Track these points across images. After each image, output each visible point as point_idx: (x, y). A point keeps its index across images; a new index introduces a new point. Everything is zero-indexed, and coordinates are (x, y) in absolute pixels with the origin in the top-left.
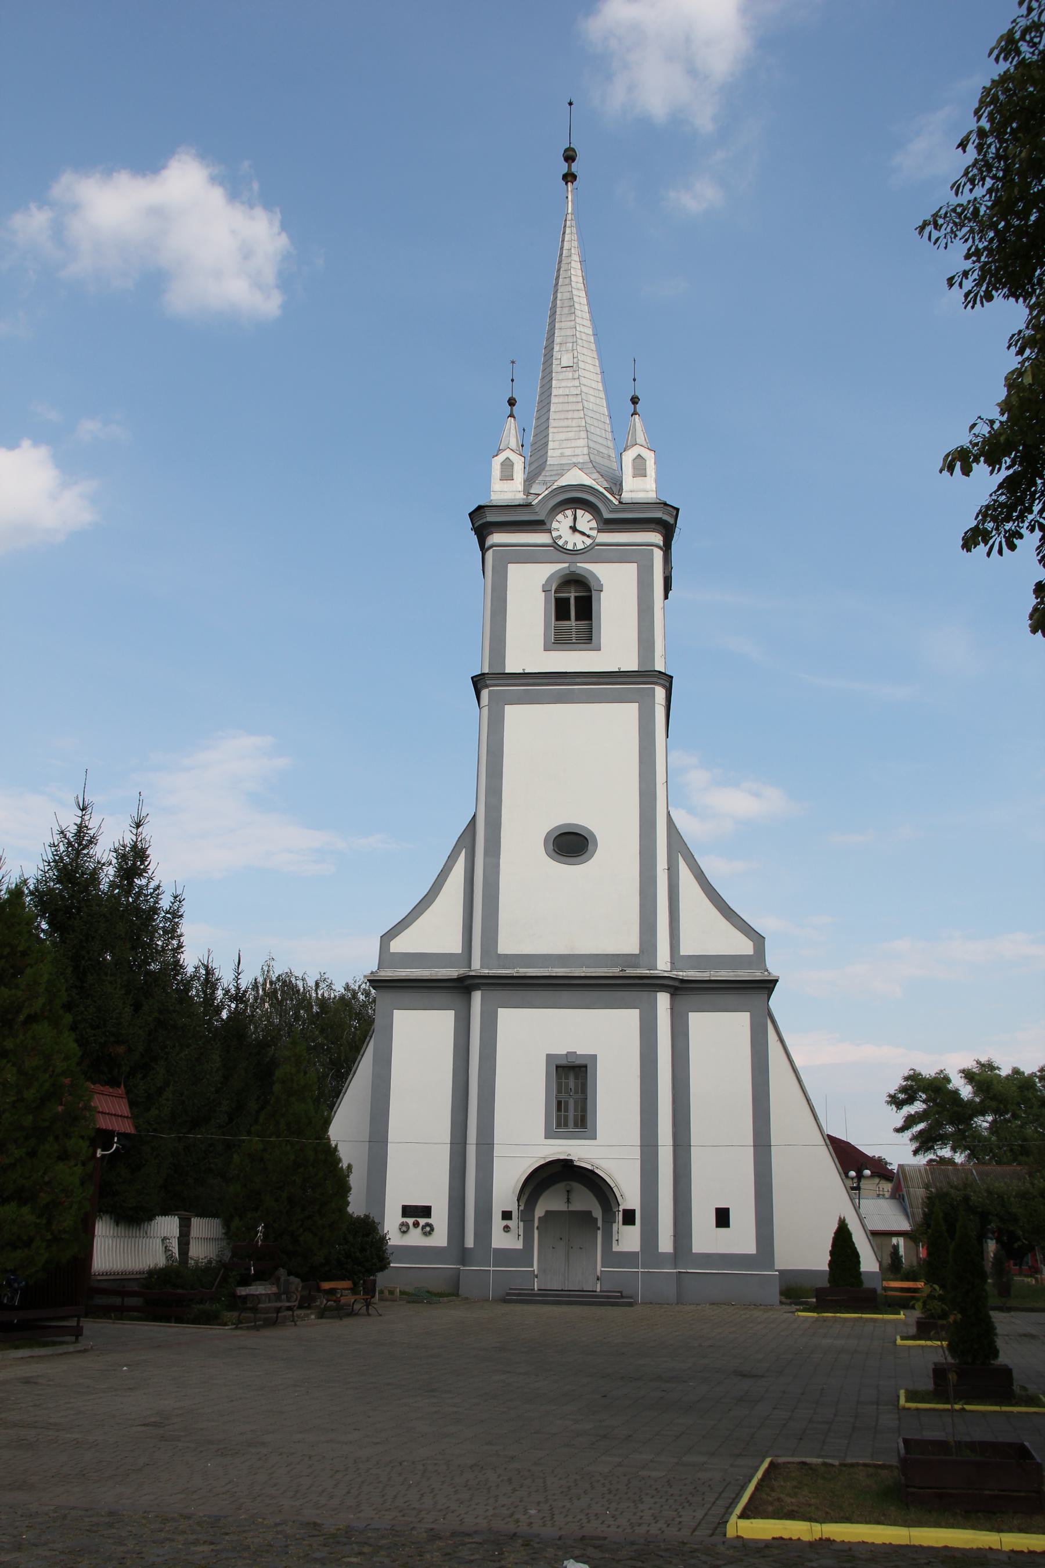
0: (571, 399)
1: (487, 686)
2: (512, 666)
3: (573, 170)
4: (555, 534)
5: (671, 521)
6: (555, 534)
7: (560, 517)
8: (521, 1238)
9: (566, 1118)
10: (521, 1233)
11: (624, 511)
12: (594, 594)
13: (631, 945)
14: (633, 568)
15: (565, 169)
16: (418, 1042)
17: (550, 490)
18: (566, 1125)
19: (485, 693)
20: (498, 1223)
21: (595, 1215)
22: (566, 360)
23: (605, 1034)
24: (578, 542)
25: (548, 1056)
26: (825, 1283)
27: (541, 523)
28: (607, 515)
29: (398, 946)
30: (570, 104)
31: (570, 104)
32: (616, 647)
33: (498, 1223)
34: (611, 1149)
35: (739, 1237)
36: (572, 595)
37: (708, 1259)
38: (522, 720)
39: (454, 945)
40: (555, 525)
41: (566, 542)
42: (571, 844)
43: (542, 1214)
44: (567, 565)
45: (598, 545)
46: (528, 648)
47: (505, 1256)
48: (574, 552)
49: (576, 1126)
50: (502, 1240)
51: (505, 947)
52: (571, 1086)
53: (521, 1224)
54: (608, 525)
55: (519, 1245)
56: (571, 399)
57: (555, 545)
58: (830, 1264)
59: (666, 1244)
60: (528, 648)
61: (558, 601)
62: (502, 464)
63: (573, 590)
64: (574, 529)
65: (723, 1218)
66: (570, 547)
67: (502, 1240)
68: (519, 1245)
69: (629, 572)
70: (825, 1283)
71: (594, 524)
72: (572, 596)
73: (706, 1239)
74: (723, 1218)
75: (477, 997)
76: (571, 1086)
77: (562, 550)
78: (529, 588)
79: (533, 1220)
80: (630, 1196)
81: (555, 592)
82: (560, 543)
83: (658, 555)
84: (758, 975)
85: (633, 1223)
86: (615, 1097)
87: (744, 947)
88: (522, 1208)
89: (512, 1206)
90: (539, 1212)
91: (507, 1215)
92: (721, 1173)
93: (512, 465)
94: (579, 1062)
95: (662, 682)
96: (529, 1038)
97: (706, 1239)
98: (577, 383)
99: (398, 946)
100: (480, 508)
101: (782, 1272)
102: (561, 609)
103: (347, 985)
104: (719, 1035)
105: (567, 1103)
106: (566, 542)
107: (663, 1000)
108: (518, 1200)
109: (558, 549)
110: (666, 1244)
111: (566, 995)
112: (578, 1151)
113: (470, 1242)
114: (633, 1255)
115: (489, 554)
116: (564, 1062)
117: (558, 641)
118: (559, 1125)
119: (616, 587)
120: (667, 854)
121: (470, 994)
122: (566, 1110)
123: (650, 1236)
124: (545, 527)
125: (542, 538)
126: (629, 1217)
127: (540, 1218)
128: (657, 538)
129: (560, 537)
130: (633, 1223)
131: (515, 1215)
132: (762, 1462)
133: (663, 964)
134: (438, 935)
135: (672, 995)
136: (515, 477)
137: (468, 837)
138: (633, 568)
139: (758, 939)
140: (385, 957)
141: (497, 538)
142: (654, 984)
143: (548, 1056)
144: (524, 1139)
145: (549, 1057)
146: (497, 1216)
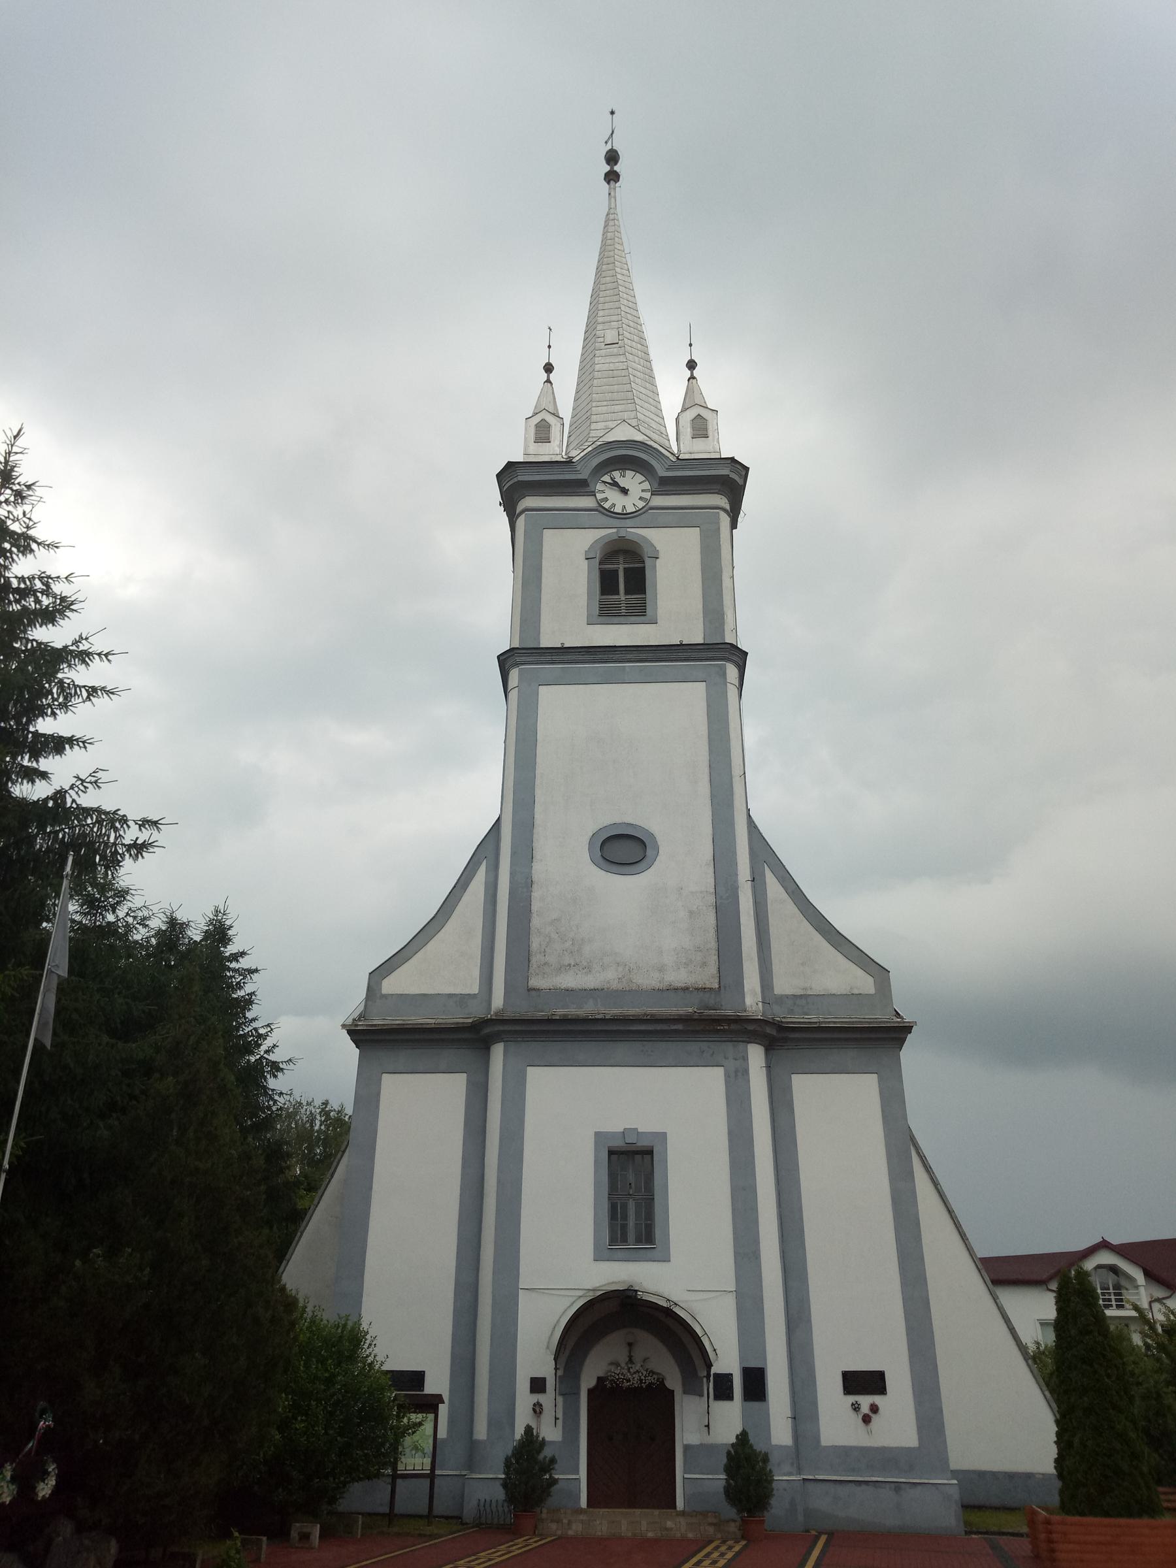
0: (619, 373)
1: (517, 665)
2: (547, 640)
3: (616, 168)
4: (599, 496)
5: (740, 482)
6: (599, 496)
8: (560, 1422)
9: (624, 1227)
10: (560, 1415)
11: (683, 468)
12: (648, 563)
13: (707, 976)
14: (778, 990)
15: (608, 168)
17: (594, 446)
18: (624, 1240)
19: (514, 675)
20: (524, 1400)
21: (669, 1384)
22: (611, 336)
23: (679, 1103)
24: (629, 503)
25: (597, 1134)
28: (662, 472)
29: (390, 986)
30: (612, 113)
31: (612, 113)
32: (675, 615)
33: (524, 1400)
34: (691, 1273)
35: (896, 1422)
37: (845, 1454)
38: (564, 706)
41: (614, 505)
42: (623, 849)
43: (592, 1383)
44: (614, 530)
45: (651, 508)
46: (570, 621)
48: (624, 516)
49: (638, 1240)
52: (631, 1181)
53: (560, 1399)
56: (619, 373)
60: (570, 621)
62: (537, 426)
63: (621, 560)
66: (618, 509)
71: (647, 486)
72: (621, 568)
75: (498, 1052)
76: (631, 1181)
77: (610, 513)
78: (571, 555)
79: (578, 1394)
80: (727, 1359)
81: (600, 563)
82: (607, 505)
83: (725, 520)
84: (880, 1016)
85: (729, 1397)
86: (694, 1196)
87: (865, 984)
88: (560, 1373)
89: (546, 1368)
91: (537, 1385)
92: (856, 1323)
93: (549, 426)
94: (644, 1143)
95: (735, 658)
96: (570, 1109)
97: (837, 1421)
98: (622, 358)
99: (390, 986)
100: (510, 465)
102: (607, 583)
103: (326, 1103)
104: (836, 1108)
105: (625, 1207)
106: (614, 505)
107: (756, 1055)
108: (556, 1359)
111: (621, 1049)
112: (652, 1278)
113: (481, 1432)
115: (521, 522)
116: (618, 1143)
117: (607, 612)
118: (613, 1241)
119: (673, 555)
120: (746, 868)
121: (488, 1049)
122: (625, 1217)
124: (588, 489)
127: (590, 1391)
128: (722, 501)
129: (606, 499)
130: (729, 1397)
131: (550, 1384)
133: (752, 1002)
134: (451, 975)
135: (768, 1050)
136: (552, 439)
138: (778, 990)
139: (880, 973)
141: (529, 502)
143: (597, 1134)
144: (563, 1261)
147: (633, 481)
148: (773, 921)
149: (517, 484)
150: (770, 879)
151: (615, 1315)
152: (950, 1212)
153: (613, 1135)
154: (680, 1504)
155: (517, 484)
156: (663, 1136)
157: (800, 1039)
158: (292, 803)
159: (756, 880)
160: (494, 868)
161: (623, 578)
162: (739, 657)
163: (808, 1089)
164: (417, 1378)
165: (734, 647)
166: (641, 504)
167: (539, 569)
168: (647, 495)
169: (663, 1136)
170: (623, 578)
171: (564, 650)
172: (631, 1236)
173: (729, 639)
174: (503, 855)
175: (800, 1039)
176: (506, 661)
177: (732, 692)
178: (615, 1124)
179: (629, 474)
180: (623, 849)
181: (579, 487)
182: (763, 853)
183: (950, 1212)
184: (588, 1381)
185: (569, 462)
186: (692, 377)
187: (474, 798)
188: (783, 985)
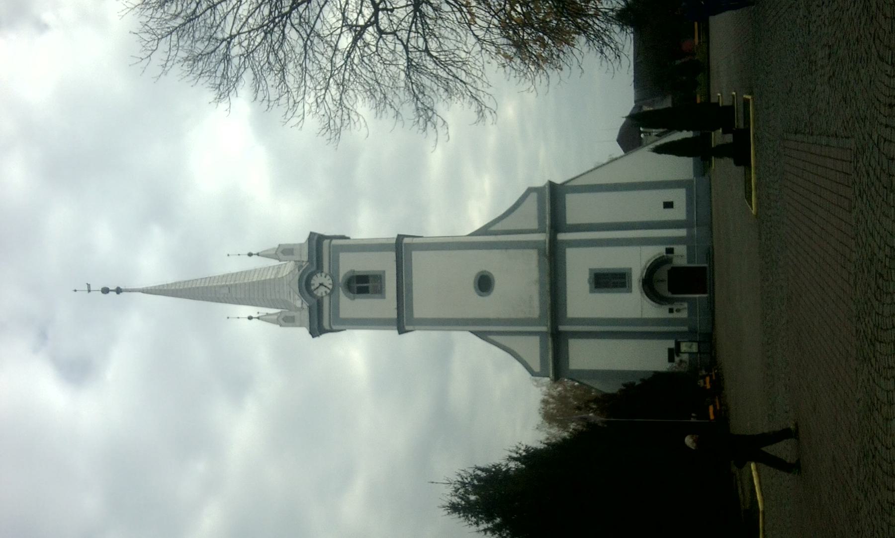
2: (394, 315)
5: (316, 237)
7: (331, 281)
13: (533, 254)
16: (585, 356)
20: (675, 315)
22: (226, 291)
23: (579, 264)
24: (328, 282)
26: (699, 159)
27: (318, 301)
28: (314, 268)
32: (385, 264)
33: (675, 315)
34: (635, 260)
35: (679, 196)
36: (355, 285)
37: (689, 212)
39: (535, 341)
40: (319, 295)
42: (484, 284)
47: (691, 311)
48: (334, 284)
49: (625, 278)
50: (684, 314)
51: (535, 313)
52: (607, 281)
54: (319, 268)
55: (686, 305)
57: (330, 295)
58: (689, 156)
59: (682, 232)
60: (387, 305)
61: (358, 293)
64: (321, 284)
65: (668, 205)
67: (684, 314)
68: (686, 305)
69: (344, 257)
70: (699, 159)
71: (319, 275)
73: (679, 213)
74: (668, 205)
75: (562, 328)
76: (607, 281)
78: (349, 305)
80: (658, 251)
83: (334, 242)
84: (547, 191)
87: (534, 195)
90: (670, 295)
91: (671, 311)
92: (647, 206)
93: (669, 290)
96: (582, 302)
99: (537, 368)
100: (310, 333)
101: (696, 174)
104: (578, 209)
107: (561, 236)
109: (332, 292)
110: (682, 232)
113: (685, 329)
114: (688, 249)
115: (334, 328)
119: (350, 264)
120: (490, 237)
123: (678, 240)
125: (326, 301)
126: (670, 251)
127: (673, 293)
128: (326, 242)
132: (764, 505)
133: (543, 237)
134: (532, 348)
137: (482, 335)
139: (530, 190)
140: (543, 374)
142: (553, 241)
144: (632, 304)
145: (591, 291)
146: (671, 316)
147: (316, 281)
148: (511, 228)
149: (317, 330)
150: (493, 228)
151: (649, 285)
152: (584, 174)
153: (591, 288)
154: (706, 265)
155: (317, 330)
156: (591, 270)
157: (556, 221)
158: (506, 410)
159: (496, 233)
160: (491, 333)
161: (362, 284)
162: (400, 238)
163: (571, 218)
164: (671, 351)
165: (397, 239)
166: (328, 277)
167: (360, 319)
168: (323, 275)
169: (591, 270)
170: (362, 284)
171: (398, 308)
172: (623, 280)
173: (394, 241)
174: (485, 329)
175: (556, 221)
176: (402, 331)
177: (415, 240)
178: (587, 287)
179: (312, 282)
180: (484, 284)
181: (320, 303)
182: (484, 231)
183: (588, 172)
184: (670, 295)
185: (310, 308)
186: (258, 254)
187: (466, 343)
188: (534, 225)
